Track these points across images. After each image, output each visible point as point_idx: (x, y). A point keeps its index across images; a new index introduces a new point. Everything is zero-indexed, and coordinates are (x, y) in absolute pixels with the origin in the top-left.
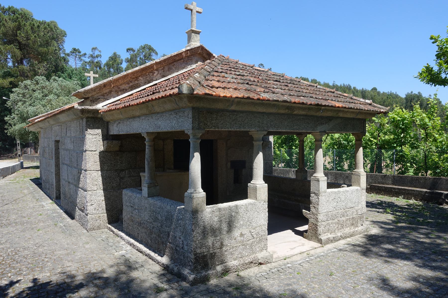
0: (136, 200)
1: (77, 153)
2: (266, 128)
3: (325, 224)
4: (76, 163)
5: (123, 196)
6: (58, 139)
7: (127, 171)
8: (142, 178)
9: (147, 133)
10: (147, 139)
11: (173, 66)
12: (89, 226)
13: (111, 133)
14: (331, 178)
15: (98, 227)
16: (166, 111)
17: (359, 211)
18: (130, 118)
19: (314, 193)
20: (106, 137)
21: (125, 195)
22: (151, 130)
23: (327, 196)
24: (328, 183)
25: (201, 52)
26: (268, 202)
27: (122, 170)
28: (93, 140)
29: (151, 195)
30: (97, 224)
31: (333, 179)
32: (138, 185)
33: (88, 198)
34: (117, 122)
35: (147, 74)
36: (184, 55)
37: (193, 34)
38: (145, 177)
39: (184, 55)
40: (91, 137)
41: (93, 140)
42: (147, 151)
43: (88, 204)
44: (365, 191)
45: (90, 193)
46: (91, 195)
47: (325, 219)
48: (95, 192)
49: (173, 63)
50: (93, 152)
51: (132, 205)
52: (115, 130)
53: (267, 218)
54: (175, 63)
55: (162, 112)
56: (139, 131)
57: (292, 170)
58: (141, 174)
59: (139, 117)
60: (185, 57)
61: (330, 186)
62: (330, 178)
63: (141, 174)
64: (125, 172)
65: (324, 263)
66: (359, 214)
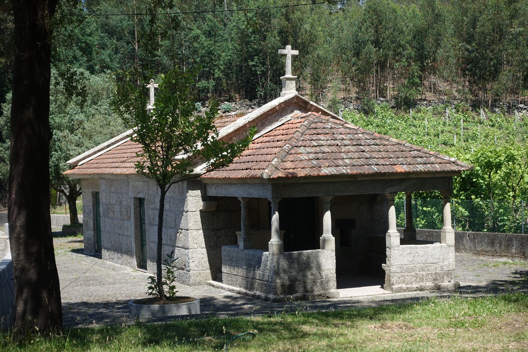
0: (234, 254)
1: (175, 213)
2: (332, 194)
3: (400, 275)
4: (174, 223)
5: (222, 252)
6: (141, 196)
7: (223, 231)
8: (238, 237)
9: (242, 198)
10: (242, 203)
11: (267, 120)
12: (191, 281)
13: (210, 194)
14: (516, 244)
15: (199, 283)
16: (255, 184)
17: (445, 267)
18: (227, 184)
19: (388, 247)
20: (205, 198)
21: (225, 250)
22: (245, 196)
23: (400, 250)
24: (401, 239)
25: (296, 101)
26: (336, 251)
27: (219, 230)
28: (193, 201)
29: (246, 248)
30: (198, 280)
31: (519, 246)
32: (235, 243)
33: (190, 256)
34: (215, 186)
35: (241, 133)
36: (278, 108)
37: (288, 82)
38: (241, 235)
39: (277, 108)
40: (191, 198)
41: (193, 201)
42: (242, 212)
43: (191, 261)
44: (453, 249)
45: (191, 250)
46: (192, 253)
47: (399, 271)
48: (196, 249)
49: (266, 117)
50: (193, 213)
51: (230, 258)
52: (212, 192)
53: (335, 264)
54: (269, 117)
55: (253, 184)
56: (236, 196)
57: (466, 233)
58: (237, 233)
59: (235, 184)
60: (279, 109)
61: (403, 242)
62: (515, 245)
63: (237, 233)
64: (222, 232)
65: (434, 334)
66: (445, 270)
